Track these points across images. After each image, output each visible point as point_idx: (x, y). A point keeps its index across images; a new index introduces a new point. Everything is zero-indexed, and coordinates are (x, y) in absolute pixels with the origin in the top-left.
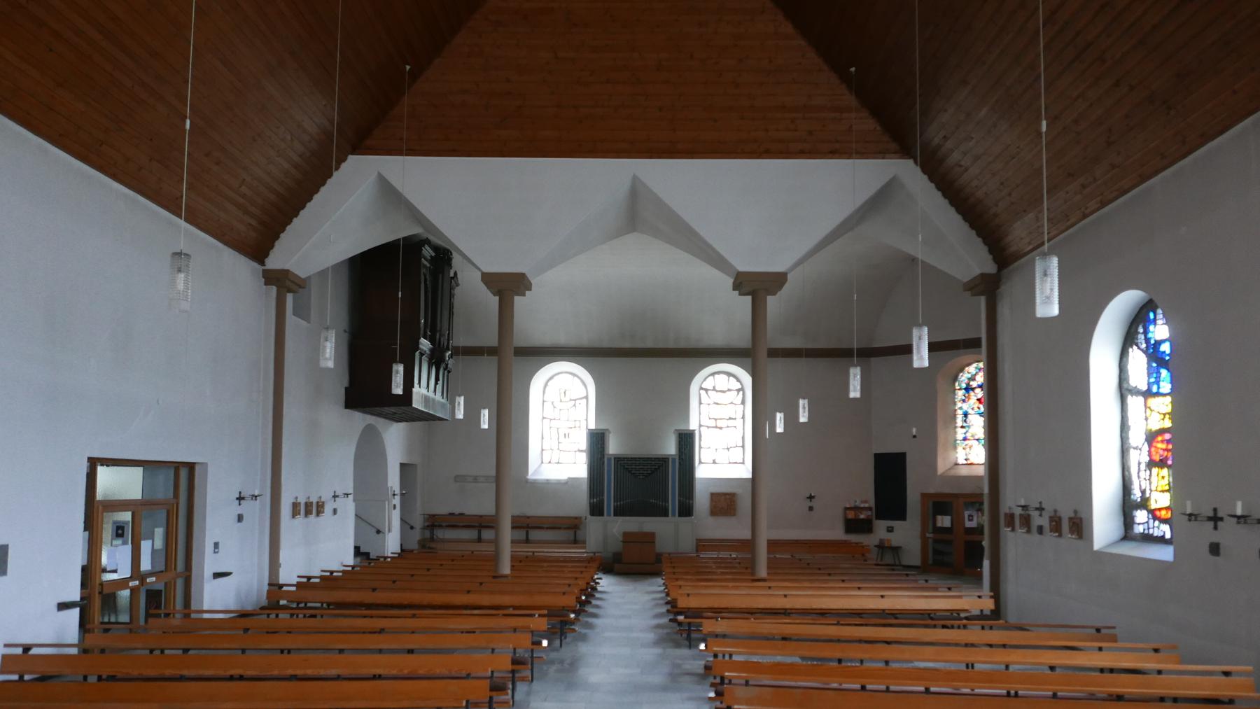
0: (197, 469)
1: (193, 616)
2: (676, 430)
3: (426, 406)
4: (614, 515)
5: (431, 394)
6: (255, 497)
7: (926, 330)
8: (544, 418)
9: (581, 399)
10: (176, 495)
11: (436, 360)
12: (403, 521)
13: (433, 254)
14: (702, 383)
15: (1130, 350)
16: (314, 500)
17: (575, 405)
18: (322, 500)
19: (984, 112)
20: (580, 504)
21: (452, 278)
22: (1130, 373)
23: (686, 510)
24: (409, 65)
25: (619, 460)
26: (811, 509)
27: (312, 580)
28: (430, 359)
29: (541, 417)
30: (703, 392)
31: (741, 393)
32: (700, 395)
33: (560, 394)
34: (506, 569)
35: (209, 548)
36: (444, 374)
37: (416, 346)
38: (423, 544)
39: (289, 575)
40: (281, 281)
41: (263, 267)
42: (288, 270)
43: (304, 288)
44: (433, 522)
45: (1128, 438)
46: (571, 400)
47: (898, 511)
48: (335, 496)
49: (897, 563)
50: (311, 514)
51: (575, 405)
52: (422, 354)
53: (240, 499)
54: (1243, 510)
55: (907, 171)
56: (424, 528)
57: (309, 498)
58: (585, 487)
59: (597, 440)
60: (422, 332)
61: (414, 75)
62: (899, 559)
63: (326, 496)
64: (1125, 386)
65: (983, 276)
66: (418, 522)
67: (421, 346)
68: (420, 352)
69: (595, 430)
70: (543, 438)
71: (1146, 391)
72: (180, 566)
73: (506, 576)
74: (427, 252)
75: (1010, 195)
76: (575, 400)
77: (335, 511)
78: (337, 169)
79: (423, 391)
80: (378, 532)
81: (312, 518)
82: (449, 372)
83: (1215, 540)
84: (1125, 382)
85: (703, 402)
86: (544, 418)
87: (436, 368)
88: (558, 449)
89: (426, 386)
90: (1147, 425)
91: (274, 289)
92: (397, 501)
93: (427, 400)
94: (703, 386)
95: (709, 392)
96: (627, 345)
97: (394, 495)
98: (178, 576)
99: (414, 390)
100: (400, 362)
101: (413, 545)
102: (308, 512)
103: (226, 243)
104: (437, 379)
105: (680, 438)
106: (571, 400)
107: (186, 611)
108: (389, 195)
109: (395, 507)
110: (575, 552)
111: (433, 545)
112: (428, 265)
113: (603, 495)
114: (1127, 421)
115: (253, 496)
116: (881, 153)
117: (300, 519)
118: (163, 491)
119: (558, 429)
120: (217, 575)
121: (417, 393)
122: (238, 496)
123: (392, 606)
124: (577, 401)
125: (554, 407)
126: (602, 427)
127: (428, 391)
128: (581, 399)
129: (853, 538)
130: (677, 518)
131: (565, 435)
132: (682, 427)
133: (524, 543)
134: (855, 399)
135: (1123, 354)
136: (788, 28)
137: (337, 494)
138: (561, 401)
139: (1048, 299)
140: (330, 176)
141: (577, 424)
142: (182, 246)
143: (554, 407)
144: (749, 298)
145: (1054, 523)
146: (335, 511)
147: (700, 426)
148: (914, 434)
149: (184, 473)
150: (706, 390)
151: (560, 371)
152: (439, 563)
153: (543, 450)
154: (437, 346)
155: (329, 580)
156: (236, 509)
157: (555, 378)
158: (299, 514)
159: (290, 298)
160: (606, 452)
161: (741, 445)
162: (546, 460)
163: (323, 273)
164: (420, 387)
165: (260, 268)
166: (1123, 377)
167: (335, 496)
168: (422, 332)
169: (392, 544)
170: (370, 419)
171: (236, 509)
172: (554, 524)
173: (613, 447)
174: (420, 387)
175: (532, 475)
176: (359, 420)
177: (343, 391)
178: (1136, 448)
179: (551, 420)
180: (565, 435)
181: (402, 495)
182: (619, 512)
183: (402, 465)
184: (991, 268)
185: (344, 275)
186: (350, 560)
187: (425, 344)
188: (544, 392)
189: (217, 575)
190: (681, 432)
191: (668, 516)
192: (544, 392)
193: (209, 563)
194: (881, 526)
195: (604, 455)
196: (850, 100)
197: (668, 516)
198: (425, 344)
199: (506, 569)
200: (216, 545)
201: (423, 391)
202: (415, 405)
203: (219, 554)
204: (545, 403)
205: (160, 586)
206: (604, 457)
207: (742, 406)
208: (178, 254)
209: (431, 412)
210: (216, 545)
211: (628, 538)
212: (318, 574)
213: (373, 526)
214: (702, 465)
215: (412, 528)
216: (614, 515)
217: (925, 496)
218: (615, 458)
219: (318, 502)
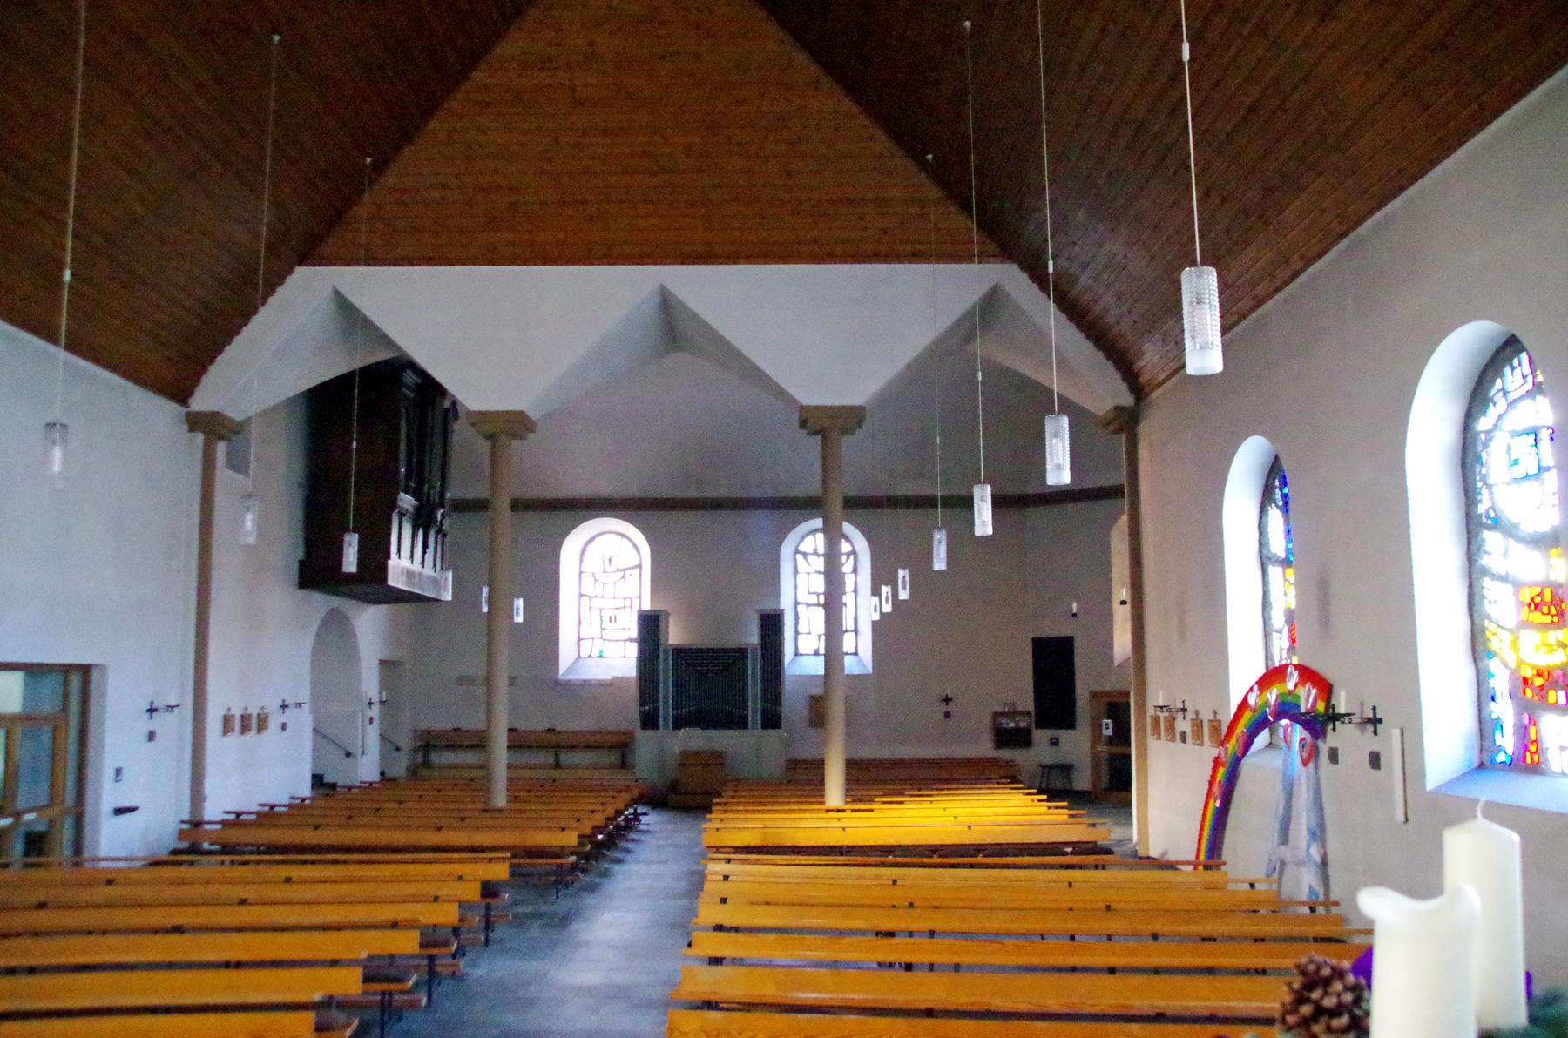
0: (95, 674)
1: (88, 865)
2: (757, 610)
3: (409, 584)
4: (763, 728)
5: (417, 567)
6: (300, 705)
7: (988, 488)
8: (581, 595)
9: (633, 568)
10: (65, 708)
11: (423, 520)
12: (383, 737)
13: (419, 381)
14: (798, 546)
15: (1269, 508)
16: (254, 712)
17: (623, 577)
18: (266, 711)
19: (1081, 214)
20: (627, 714)
21: (448, 410)
22: (1270, 536)
23: (772, 720)
24: (370, 157)
25: (679, 651)
26: (947, 715)
27: (243, 817)
28: (414, 520)
29: (577, 593)
30: (799, 557)
31: (852, 557)
32: (795, 560)
33: (604, 561)
34: (500, 799)
35: (108, 774)
36: (436, 538)
37: (392, 505)
38: (414, 771)
39: (214, 811)
40: (210, 427)
41: (186, 410)
42: (218, 412)
43: (239, 433)
44: (429, 743)
45: (1270, 619)
46: (618, 570)
47: (1068, 721)
48: (284, 707)
49: (1068, 787)
50: (250, 730)
51: (623, 577)
52: (402, 515)
53: (152, 710)
54: (1346, 704)
55: (1011, 277)
56: (415, 750)
57: (246, 708)
58: (633, 692)
59: (650, 624)
60: (402, 483)
61: (380, 167)
62: (1070, 783)
63: (272, 705)
64: (1265, 552)
65: (1119, 410)
66: (405, 740)
67: (400, 504)
68: (399, 512)
69: (651, 611)
70: (580, 623)
71: (1284, 560)
72: (70, 801)
73: (500, 810)
74: (410, 378)
75: (1130, 311)
76: (624, 570)
77: (284, 727)
78: (263, 304)
79: (405, 563)
80: (348, 754)
81: (252, 736)
82: (444, 535)
83: (1376, 749)
84: (1265, 548)
85: (800, 570)
86: (581, 595)
87: (423, 529)
88: (601, 638)
89: (409, 556)
90: (1286, 601)
91: (200, 438)
92: (375, 711)
93: (410, 575)
94: (801, 548)
95: (809, 557)
96: (692, 493)
97: (370, 704)
98: (67, 812)
99: (391, 563)
100: (355, 532)
101: (399, 768)
102: (245, 728)
103: (139, 381)
104: (425, 546)
105: (762, 620)
106: (618, 570)
107: (76, 859)
108: (349, 316)
109: (371, 720)
110: (620, 778)
111: (426, 773)
112: (412, 395)
113: (658, 701)
114: (1269, 596)
115: (169, 706)
116: (983, 257)
117: (234, 738)
118: (49, 705)
119: (600, 610)
120: (119, 811)
121: (394, 567)
122: (148, 708)
123: (348, 850)
124: (628, 572)
125: (596, 580)
126: (658, 607)
127: (412, 562)
128: (633, 568)
129: (1006, 754)
130: (759, 731)
131: (610, 617)
132: (768, 606)
133: (552, 768)
134: (940, 572)
135: (1263, 512)
136: (848, 105)
137: (286, 703)
138: (605, 572)
139: (1059, 468)
140: (255, 311)
141: (627, 602)
142: (56, 415)
143: (596, 580)
144: (820, 437)
145: (1196, 728)
146: (284, 727)
147: (796, 603)
148: (1075, 611)
149: (75, 680)
150: (805, 555)
151: (600, 531)
152: (418, 793)
153: (580, 639)
154: (424, 503)
155: (268, 816)
156: (145, 724)
157: (597, 540)
158: (233, 730)
159: (221, 448)
160: (662, 640)
161: (853, 628)
162: (584, 653)
163: (268, 413)
164: (399, 557)
165: (183, 410)
166: (1262, 541)
167: (284, 707)
168: (402, 483)
169: (367, 769)
170: (336, 602)
171: (145, 724)
172: (593, 743)
173: (675, 634)
174: (399, 557)
175: (563, 674)
176: (320, 603)
177: (295, 567)
178: (1277, 631)
179: (591, 597)
180: (610, 617)
181: (382, 703)
182: (679, 723)
183: (383, 663)
184: (1127, 400)
185: (300, 416)
186: (305, 790)
187: (407, 501)
188: (581, 561)
189: (119, 811)
190: (764, 613)
191: (658, 728)
192: (581, 561)
193: (106, 794)
194: (1041, 736)
195: (658, 645)
196: (933, 192)
197: (658, 728)
198: (407, 501)
199: (500, 799)
200: (118, 772)
201: (405, 563)
202: (392, 582)
203: (121, 783)
204: (583, 575)
205: (41, 827)
206: (658, 648)
207: (853, 575)
208: (51, 426)
209: (416, 591)
210: (118, 772)
211: (688, 759)
212: (255, 808)
213: (339, 746)
214: (802, 658)
215: (398, 749)
216: (763, 728)
217: (1095, 695)
218: (673, 650)
219: (259, 715)
